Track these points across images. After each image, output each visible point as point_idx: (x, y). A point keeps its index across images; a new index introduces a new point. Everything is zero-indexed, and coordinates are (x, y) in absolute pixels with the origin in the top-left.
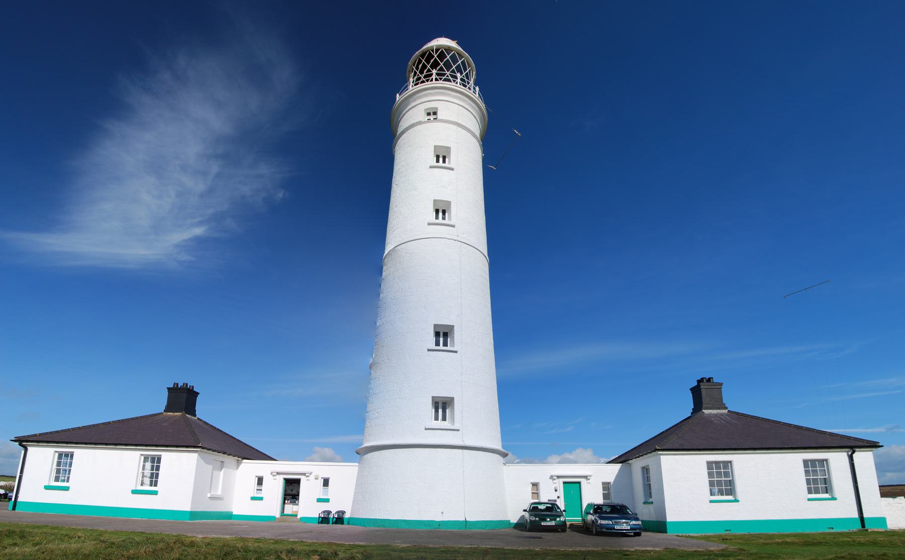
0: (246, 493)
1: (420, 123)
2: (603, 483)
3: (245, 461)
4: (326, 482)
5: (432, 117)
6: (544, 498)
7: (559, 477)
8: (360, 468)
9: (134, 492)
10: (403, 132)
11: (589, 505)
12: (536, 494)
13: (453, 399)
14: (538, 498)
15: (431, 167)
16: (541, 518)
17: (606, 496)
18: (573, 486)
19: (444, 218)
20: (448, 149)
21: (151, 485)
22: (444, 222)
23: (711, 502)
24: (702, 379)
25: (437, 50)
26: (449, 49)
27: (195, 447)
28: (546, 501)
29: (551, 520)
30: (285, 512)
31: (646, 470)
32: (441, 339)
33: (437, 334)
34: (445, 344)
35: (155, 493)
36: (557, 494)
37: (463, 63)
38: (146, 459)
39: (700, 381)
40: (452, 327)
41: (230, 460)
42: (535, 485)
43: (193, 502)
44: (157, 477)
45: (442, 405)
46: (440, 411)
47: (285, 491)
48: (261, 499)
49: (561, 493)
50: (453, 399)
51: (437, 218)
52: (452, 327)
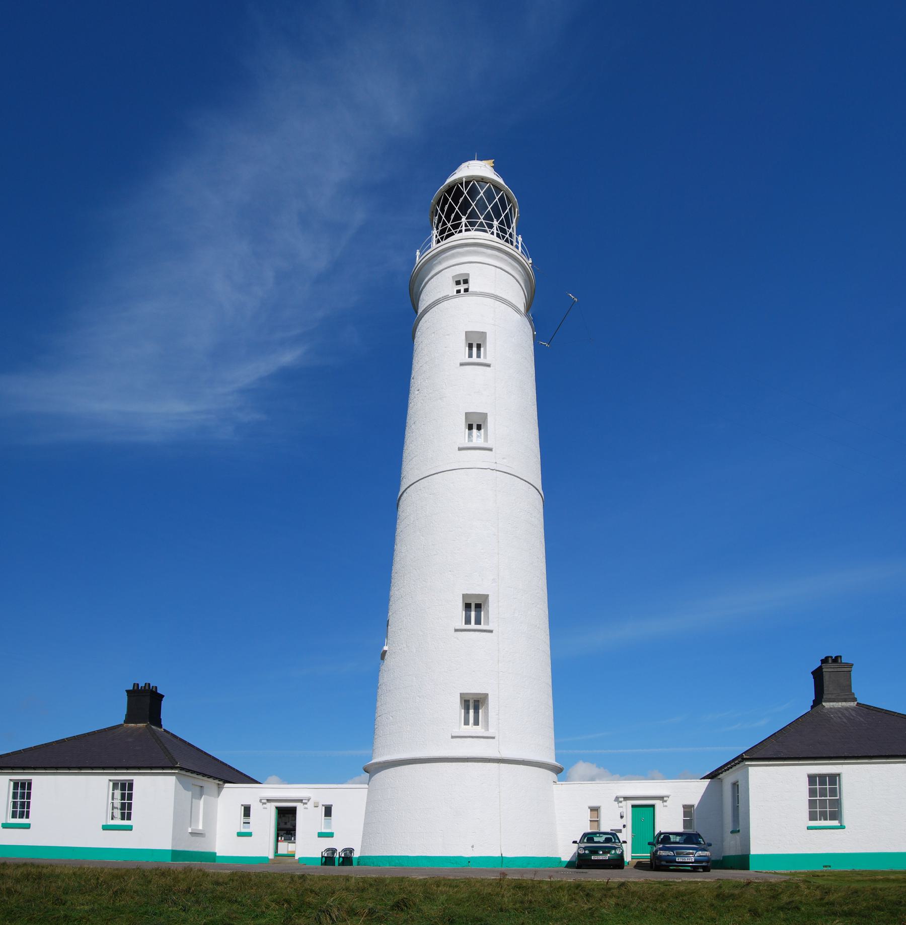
0: (231, 828)
1: (446, 298)
2: (685, 807)
3: (227, 785)
4: (328, 811)
5: (462, 287)
6: (605, 827)
7: (626, 798)
8: (369, 791)
9: (106, 828)
10: (425, 311)
11: (660, 834)
12: (595, 822)
13: (487, 695)
14: (599, 826)
15: (462, 364)
16: (596, 852)
17: (686, 824)
18: (644, 810)
19: (479, 356)
20: (483, 335)
21: (123, 818)
22: (478, 360)
23: (808, 828)
24: (827, 658)
25: (467, 183)
26: (482, 180)
27: (172, 768)
28: (609, 831)
29: (604, 853)
30: (280, 852)
31: (735, 785)
32: (473, 614)
33: (468, 606)
34: (478, 622)
35: (130, 828)
36: (623, 821)
37: (501, 199)
38: (115, 786)
39: (825, 661)
40: (486, 696)
41: (210, 784)
42: (595, 810)
43: (174, 839)
44: (130, 808)
45: (474, 705)
46: (471, 712)
47: (278, 824)
48: (249, 835)
49: (628, 820)
50: (487, 695)
51: (470, 356)
52: (486, 696)
